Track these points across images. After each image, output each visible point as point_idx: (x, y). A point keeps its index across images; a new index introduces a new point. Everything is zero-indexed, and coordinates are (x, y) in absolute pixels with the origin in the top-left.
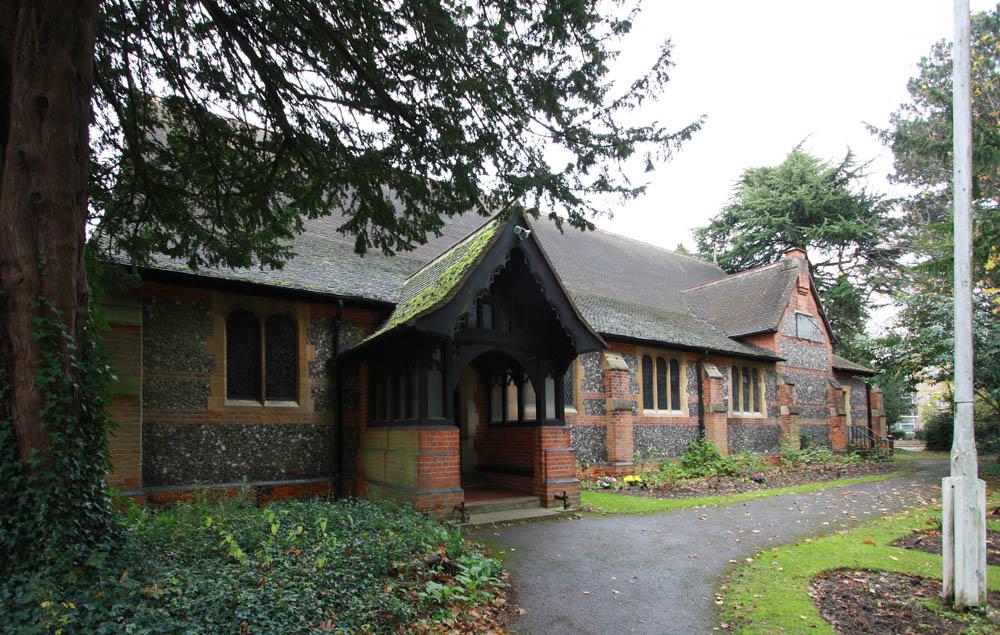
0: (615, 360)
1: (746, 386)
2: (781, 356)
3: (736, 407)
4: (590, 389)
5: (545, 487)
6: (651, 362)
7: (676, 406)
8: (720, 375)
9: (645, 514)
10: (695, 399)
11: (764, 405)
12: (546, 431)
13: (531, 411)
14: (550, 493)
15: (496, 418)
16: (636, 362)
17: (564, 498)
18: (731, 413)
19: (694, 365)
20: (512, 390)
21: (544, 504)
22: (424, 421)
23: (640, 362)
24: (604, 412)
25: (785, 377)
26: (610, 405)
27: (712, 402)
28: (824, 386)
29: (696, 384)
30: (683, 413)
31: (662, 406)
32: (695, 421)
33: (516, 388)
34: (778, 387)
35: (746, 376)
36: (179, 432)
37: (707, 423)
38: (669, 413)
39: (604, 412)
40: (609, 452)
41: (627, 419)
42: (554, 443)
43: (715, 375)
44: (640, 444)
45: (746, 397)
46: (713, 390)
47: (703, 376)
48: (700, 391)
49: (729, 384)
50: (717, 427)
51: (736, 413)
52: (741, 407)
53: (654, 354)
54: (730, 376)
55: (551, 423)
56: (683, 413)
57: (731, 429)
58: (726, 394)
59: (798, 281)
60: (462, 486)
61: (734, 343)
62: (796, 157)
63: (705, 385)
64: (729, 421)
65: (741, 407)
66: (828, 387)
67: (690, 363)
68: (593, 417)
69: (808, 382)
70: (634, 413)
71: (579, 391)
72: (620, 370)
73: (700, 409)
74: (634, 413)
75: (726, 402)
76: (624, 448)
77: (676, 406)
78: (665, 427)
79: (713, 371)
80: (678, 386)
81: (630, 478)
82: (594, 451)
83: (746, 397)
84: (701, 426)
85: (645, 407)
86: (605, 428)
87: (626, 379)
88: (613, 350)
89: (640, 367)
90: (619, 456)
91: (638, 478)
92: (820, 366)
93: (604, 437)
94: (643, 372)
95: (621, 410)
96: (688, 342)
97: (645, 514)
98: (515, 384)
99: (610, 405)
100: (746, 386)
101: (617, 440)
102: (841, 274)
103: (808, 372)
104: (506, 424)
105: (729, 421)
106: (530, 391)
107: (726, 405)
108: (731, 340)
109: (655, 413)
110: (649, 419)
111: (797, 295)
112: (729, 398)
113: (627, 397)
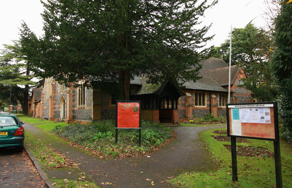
0: (188, 94)
1: (223, 99)
2: (234, 92)
3: (220, 105)
4: (182, 101)
5: (174, 121)
6: (201, 94)
7: (204, 105)
8: (216, 97)
9: (193, 126)
10: (209, 103)
11: (206, 102)
12: (174, 111)
13: (170, 106)
14: (175, 122)
15: (161, 108)
16: (193, 95)
17: (178, 123)
18: (219, 107)
19: (209, 95)
20: (166, 102)
21: (173, 124)
22: (153, 109)
23: (194, 94)
24: (185, 106)
25: (235, 97)
26: (187, 105)
27: (213, 104)
28: (248, 99)
29: (209, 99)
30: (205, 106)
31: (200, 105)
32: (209, 108)
33: (167, 102)
34: (233, 100)
35: (223, 96)
36: (104, 111)
37: (212, 109)
38: (202, 106)
39: (185, 106)
40: (186, 116)
41: (191, 108)
42: (176, 113)
43: (214, 97)
44: (194, 113)
45: (223, 102)
46: (214, 102)
47: (211, 97)
48: (210, 101)
49: (218, 99)
50: (214, 110)
51: (220, 107)
52: (222, 105)
53: (198, 92)
54: (219, 97)
55: (175, 109)
56: (205, 106)
57: (219, 111)
58: (217, 102)
59: (240, 71)
60: (159, 120)
61: (222, 88)
62: (250, 27)
63: (211, 100)
64: (218, 109)
65: (222, 105)
66: (249, 99)
67: (207, 94)
68: (183, 108)
69: (243, 98)
70: (193, 107)
71: (179, 102)
72: (189, 97)
73: (210, 106)
74: (193, 107)
75: (217, 104)
76: (190, 115)
77: (204, 105)
78: (200, 110)
79: (214, 96)
80: (204, 100)
81: (191, 121)
82: (183, 116)
83: (223, 102)
84: (210, 110)
85: (195, 105)
86: (185, 110)
87: (191, 99)
88: (188, 92)
89: (194, 96)
90: (189, 116)
91: (192, 121)
92: (247, 93)
93: (185, 112)
94: (195, 97)
95: (189, 106)
96: (207, 89)
97: (193, 126)
98: (171, 101)
99: (187, 105)
100: (223, 99)
101: (188, 113)
102: (109, 135)
103: (242, 95)
104: (164, 109)
105: (218, 109)
106: (170, 102)
107: (218, 104)
108: (221, 87)
109: (198, 106)
110: (197, 108)
111: (240, 75)
112: (218, 103)
113: (191, 103)
